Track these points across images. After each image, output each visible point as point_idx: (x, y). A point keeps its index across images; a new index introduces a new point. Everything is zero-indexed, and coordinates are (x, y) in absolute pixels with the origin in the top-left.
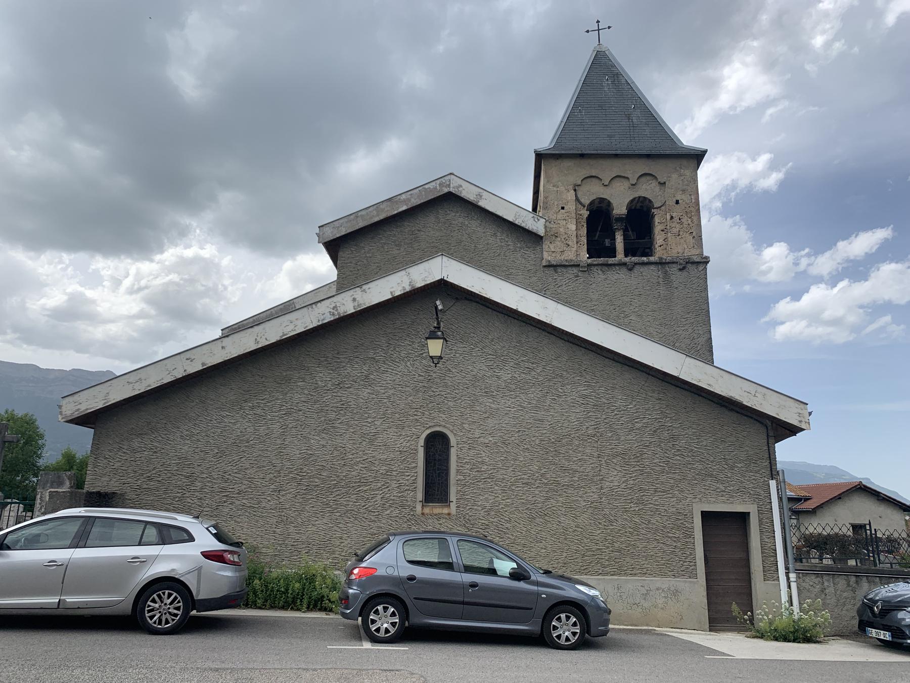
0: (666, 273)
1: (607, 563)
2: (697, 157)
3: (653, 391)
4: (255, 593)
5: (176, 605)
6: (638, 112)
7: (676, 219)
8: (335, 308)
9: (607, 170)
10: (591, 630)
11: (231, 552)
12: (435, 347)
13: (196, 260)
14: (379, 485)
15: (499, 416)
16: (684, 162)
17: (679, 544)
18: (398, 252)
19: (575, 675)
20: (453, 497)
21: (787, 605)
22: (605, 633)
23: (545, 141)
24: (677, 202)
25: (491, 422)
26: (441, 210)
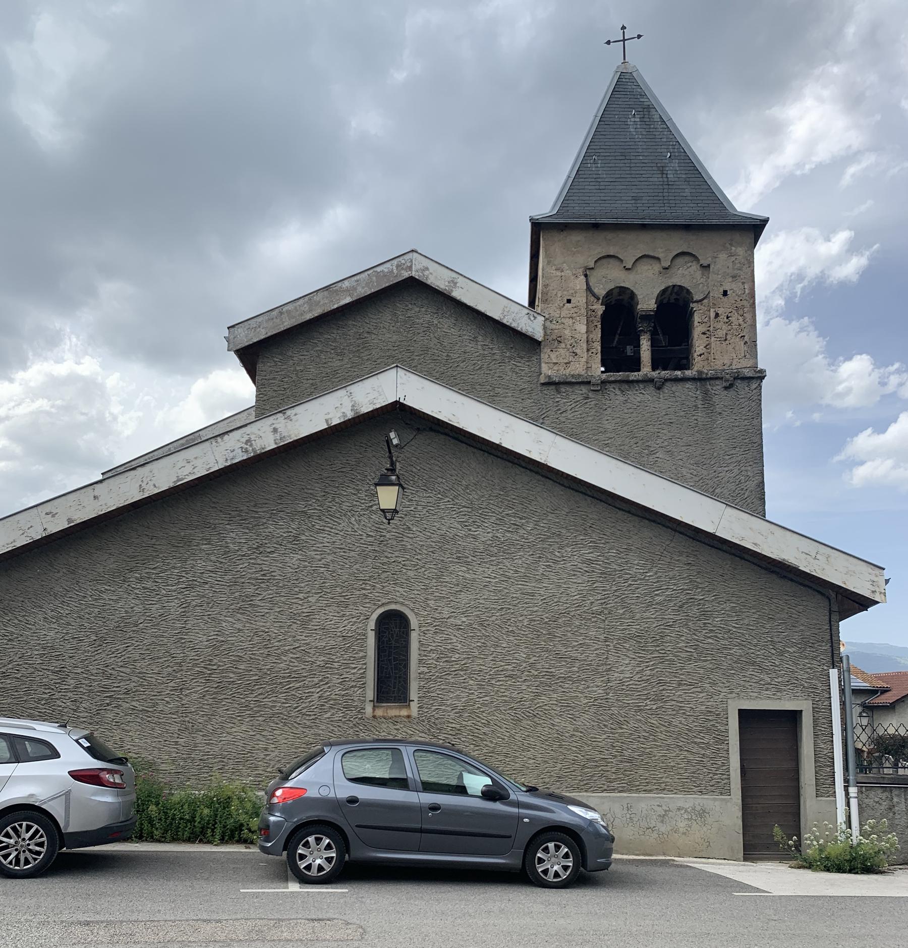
0: (706, 393)
1: (614, 776)
2: (754, 228)
3: (681, 553)
4: (151, 821)
5: (37, 839)
6: (675, 164)
8: (248, 441)
9: (631, 247)
10: (588, 863)
11: (109, 771)
12: (388, 497)
13: (71, 379)
14: (316, 680)
15: (472, 587)
16: (737, 236)
17: (708, 752)
19: (562, 921)
20: (414, 694)
21: (844, 827)
22: (606, 866)
23: (545, 200)
24: (725, 293)
25: (464, 597)
26: (399, 304)
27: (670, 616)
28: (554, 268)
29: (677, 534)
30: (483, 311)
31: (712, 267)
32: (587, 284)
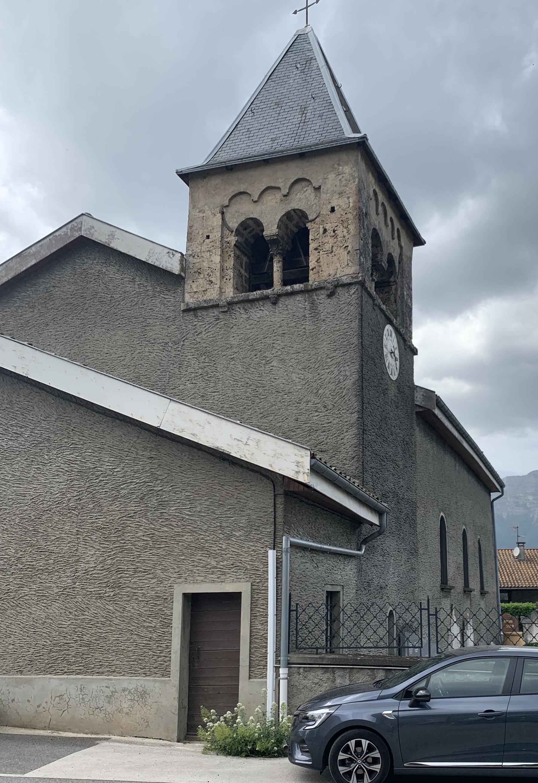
0: (313, 303)
7: (330, 232)
17: (154, 636)
18: (31, 314)
24: (333, 210)
27: (132, 507)
28: (197, 211)
29: (143, 431)
30: (133, 255)
31: (322, 187)
32: (223, 219)
